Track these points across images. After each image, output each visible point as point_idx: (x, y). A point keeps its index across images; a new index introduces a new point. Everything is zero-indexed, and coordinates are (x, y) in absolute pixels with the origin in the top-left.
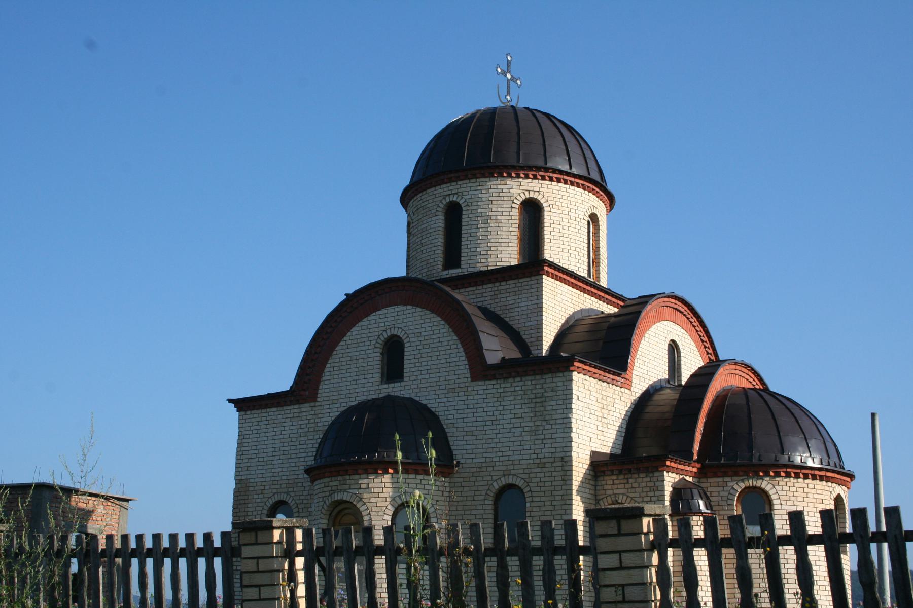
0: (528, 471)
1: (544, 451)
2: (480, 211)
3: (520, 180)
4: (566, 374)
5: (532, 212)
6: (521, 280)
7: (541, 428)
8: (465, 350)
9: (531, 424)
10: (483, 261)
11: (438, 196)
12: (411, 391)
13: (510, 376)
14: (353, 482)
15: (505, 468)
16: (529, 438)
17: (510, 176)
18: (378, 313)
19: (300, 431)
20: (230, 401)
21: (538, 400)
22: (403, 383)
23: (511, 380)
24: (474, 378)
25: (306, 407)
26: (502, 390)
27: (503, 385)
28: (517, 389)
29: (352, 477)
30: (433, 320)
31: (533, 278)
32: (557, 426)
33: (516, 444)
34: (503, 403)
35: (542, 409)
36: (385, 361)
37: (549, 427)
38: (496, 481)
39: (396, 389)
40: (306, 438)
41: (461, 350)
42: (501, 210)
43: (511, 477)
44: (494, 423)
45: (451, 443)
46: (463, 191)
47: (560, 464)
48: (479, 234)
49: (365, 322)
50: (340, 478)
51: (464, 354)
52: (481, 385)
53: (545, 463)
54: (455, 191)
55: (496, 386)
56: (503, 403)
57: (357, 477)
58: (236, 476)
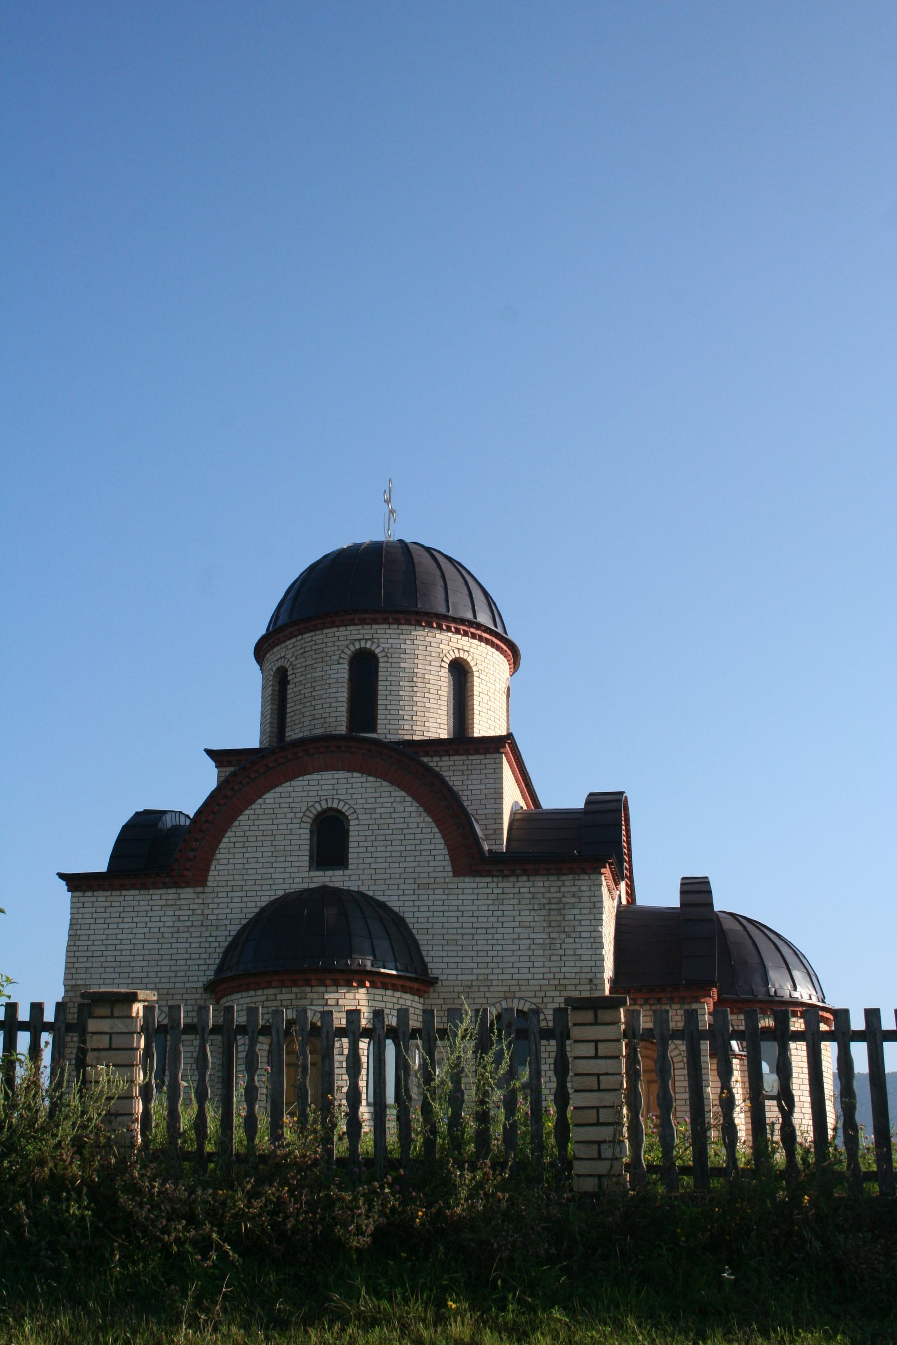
0: (542, 994)
1: (563, 970)
2: (402, 665)
3: (450, 634)
4: (593, 877)
5: (460, 672)
6: (471, 757)
7: (558, 941)
8: (443, 837)
9: (544, 935)
10: (406, 727)
11: (341, 641)
12: (360, 883)
13: (513, 873)
14: (316, 996)
15: (507, 989)
16: (541, 953)
17: (439, 627)
18: (307, 777)
19: (177, 924)
20: (62, 876)
21: (553, 906)
22: (347, 872)
23: (513, 879)
24: (459, 870)
25: (188, 893)
26: (500, 891)
27: (500, 885)
28: (522, 890)
29: (315, 989)
30: (393, 794)
31: (488, 756)
32: (582, 941)
33: (522, 959)
34: (501, 907)
35: (558, 918)
36: (315, 839)
37: (571, 940)
38: (494, 1005)
39: (335, 878)
40: (187, 935)
41: (438, 835)
42: (428, 667)
43: (516, 1001)
44: (489, 931)
45: (424, 954)
46: (381, 638)
47: (588, 987)
48: (401, 693)
49: (285, 788)
50: (295, 990)
51: (442, 841)
52: (468, 883)
53: (565, 986)
54: (369, 636)
55: (490, 885)
56: (501, 907)
57: (322, 989)
58: (65, 979)
